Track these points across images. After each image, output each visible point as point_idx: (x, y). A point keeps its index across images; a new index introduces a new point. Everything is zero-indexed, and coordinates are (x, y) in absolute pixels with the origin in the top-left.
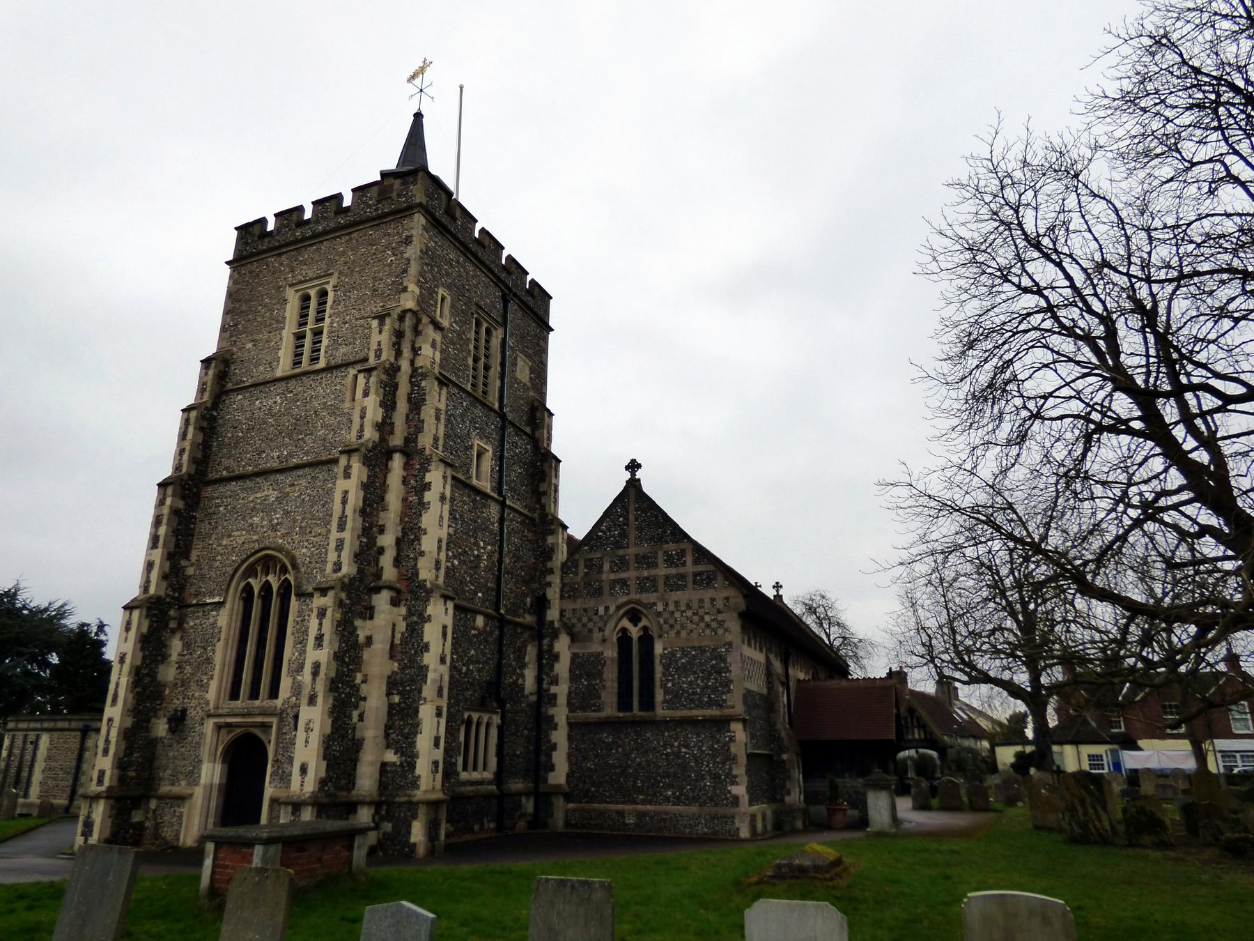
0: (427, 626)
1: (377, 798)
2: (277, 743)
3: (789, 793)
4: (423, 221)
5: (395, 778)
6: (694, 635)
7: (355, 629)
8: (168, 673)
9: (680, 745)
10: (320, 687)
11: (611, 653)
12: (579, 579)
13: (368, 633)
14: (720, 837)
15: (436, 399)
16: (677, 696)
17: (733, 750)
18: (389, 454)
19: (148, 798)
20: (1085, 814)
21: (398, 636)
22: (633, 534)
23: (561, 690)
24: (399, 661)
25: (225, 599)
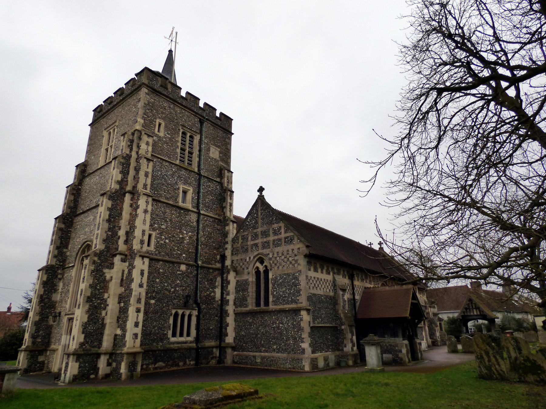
3: (345, 346)
4: (146, 91)
5: (118, 341)
6: (285, 268)
7: (104, 273)
9: (279, 323)
11: (252, 279)
12: (239, 245)
14: (295, 371)
15: (146, 167)
16: (278, 299)
17: (302, 325)
19: (46, 350)
20: (489, 361)
21: (125, 276)
22: (260, 221)
23: (231, 298)
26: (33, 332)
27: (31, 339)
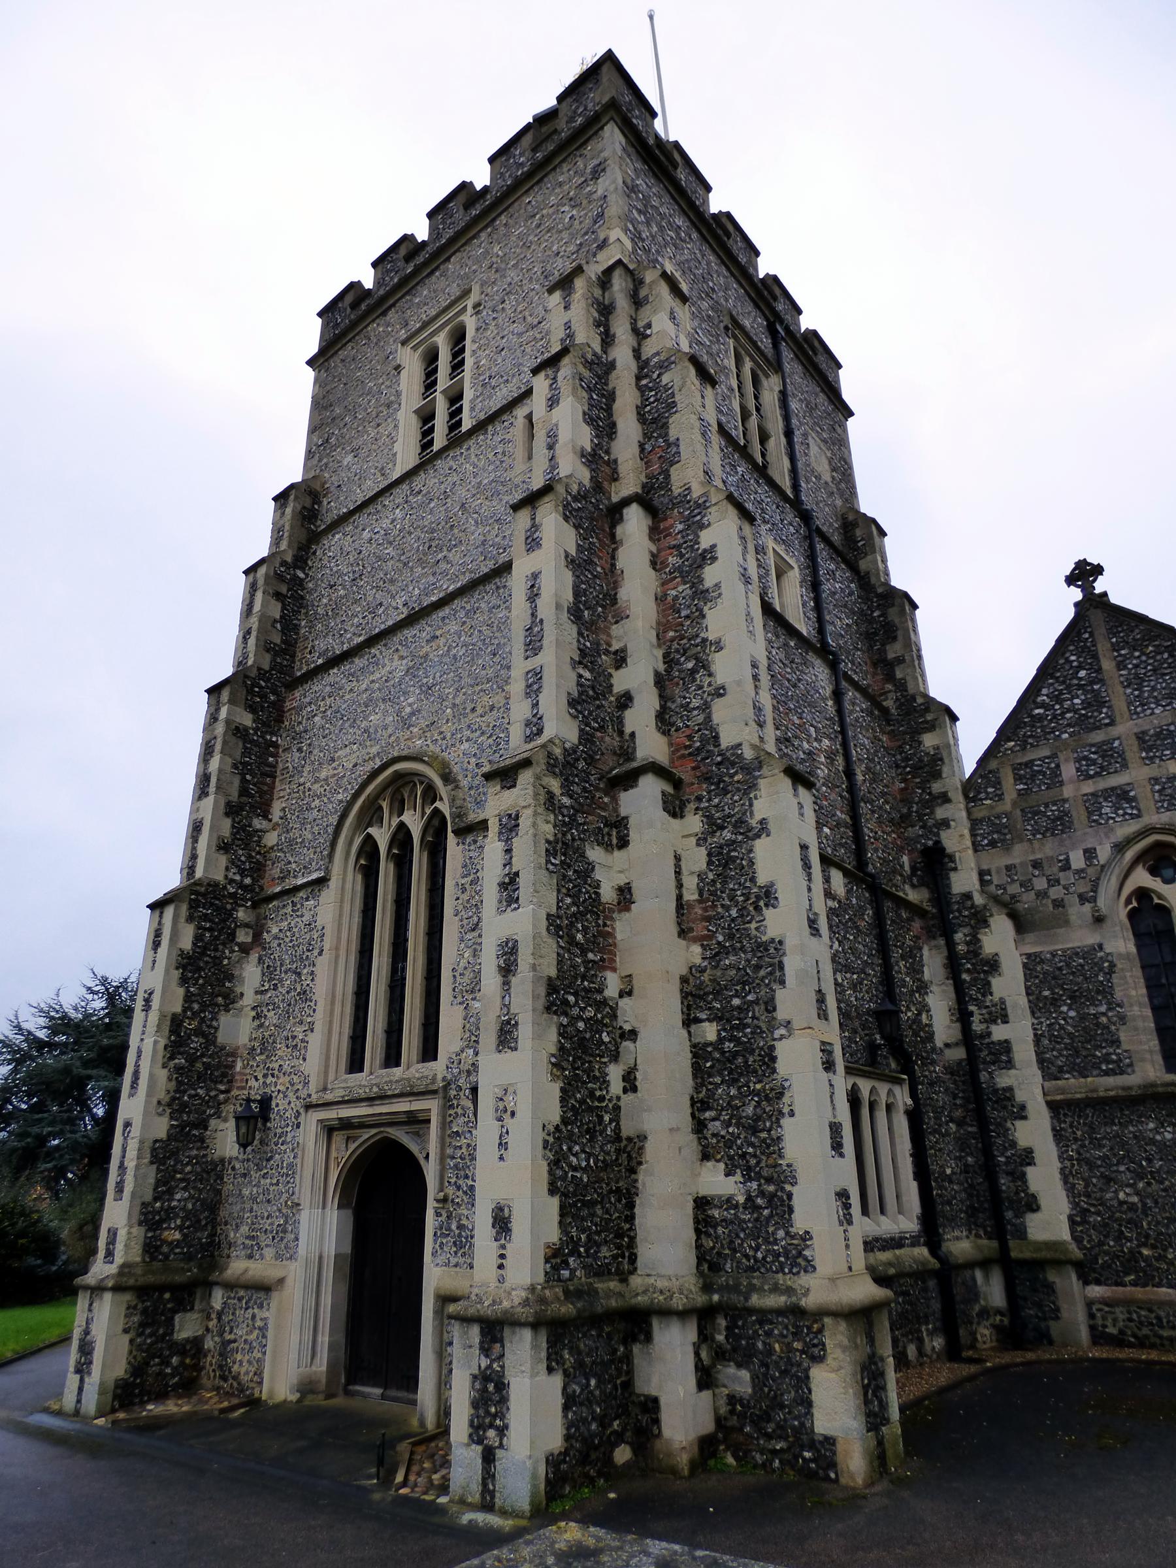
0: (761, 847)
1: (700, 1300)
2: (442, 1158)
8: (236, 1029)
10: (525, 998)
11: (1120, 943)
13: (622, 880)
18: (615, 513)
19: (209, 1285)
22: (1119, 696)
23: (1019, 1032)
24: (704, 941)
25: (328, 871)
26: (148, 1196)
27: (139, 1232)
